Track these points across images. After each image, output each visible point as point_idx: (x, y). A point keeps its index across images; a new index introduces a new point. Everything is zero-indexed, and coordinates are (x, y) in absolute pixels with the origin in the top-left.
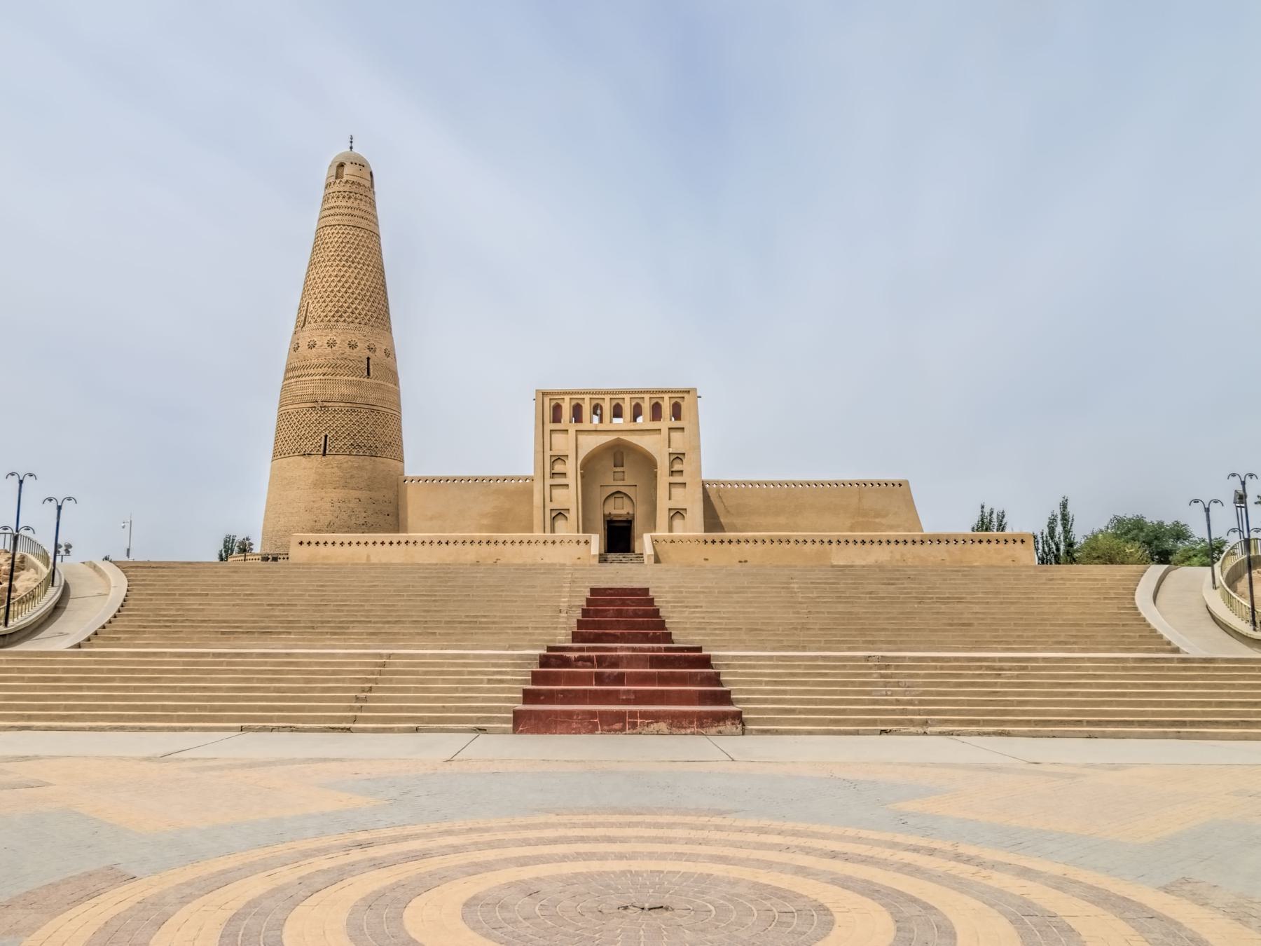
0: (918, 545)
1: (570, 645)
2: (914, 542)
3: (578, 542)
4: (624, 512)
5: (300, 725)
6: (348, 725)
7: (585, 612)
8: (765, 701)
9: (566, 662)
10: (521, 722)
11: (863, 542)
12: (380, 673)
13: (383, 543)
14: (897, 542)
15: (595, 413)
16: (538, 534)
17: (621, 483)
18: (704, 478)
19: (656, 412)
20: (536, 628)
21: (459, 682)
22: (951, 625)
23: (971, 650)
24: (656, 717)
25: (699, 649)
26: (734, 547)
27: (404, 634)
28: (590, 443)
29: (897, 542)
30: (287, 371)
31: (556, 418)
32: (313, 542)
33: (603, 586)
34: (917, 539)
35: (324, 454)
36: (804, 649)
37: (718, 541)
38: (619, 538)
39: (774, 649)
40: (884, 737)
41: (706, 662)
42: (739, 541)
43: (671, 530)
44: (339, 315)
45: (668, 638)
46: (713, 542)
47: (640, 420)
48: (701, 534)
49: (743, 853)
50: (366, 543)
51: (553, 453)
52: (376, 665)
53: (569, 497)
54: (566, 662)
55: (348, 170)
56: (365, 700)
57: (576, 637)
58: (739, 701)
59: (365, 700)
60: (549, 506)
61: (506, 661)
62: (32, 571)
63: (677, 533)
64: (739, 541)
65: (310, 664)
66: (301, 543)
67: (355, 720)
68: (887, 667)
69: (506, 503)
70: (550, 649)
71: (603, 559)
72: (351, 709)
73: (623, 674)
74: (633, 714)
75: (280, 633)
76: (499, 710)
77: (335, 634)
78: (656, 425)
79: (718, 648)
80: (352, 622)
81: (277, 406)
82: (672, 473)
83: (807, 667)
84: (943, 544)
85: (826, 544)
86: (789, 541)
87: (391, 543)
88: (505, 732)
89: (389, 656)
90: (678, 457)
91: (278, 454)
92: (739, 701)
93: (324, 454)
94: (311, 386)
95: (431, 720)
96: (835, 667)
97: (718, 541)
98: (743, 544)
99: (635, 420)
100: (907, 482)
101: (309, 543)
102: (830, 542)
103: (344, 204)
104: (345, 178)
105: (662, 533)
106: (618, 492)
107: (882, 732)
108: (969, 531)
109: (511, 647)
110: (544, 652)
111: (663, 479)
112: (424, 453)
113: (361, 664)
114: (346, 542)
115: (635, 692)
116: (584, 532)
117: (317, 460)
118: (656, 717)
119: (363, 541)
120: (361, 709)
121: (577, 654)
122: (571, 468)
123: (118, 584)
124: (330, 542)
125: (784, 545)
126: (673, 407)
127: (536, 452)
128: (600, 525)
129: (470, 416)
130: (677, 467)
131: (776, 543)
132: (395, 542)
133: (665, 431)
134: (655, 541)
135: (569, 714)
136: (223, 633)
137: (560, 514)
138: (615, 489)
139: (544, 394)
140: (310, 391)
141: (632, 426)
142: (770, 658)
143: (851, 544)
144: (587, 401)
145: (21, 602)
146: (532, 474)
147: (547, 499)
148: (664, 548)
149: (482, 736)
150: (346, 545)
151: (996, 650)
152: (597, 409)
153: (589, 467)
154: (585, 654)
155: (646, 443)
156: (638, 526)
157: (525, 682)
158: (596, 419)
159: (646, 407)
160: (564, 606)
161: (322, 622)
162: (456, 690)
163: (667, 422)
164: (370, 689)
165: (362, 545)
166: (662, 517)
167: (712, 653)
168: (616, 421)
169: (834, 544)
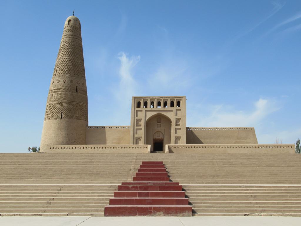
0: (257, 148)
1: (133, 182)
3: (136, 148)
5: (23, 213)
6: (41, 213)
7: (139, 170)
8: (201, 203)
9: (128, 188)
10: (109, 212)
15: (152, 105)
17: (159, 128)
18: (187, 127)
20: (121, 176)
21: (87, 196)
22: (270, 174)
23: (277, 183)
24: (159, 209)
25: (178, 183)
26: (196, 149)
27: (73, 178)
28: (149, 115)
29: (250, 147)
30: (50, 91)
31: (139, 105)
33: (147, 161)
34: (257, 146)
36: (217, 183)
37: (193, 147)
38: (158, 147)
39: (206, 183)
40: (246, 217)
41: (180, 188)
42: (197, 147)
46: (200, 147)
47: (166, 107)
48: (186, 144)
50: (72, 148)
51: (137, 118)
52: (57, 190)
53: (142, 133)
54: (128, 188)
56: (50, 203)
57: (135, 179)
59: (50, 203)
60: (136, 136)
61: (106, 188)
65: (32, 190)
66: (51, 148)
67: (45, 211)
68: (247, 190)
70: (123, 183)
71: (151, 152)
72: (44, 207)
73: (148, 193)
74: (150, 208)
75: (28, 178)
77: (48, 178)
78: (172, 108)
79: (183, 183)
80: (55, 174)
83: (218, 190)
84: (265, 148)
88: (101, 215)
89: (63, 187)
95: (74, 211)
96: (229, 190)
98: (199, 148)
100: (253, 128)
102: (228, 147)
106: (159, 131)
107: (245, 215)
109: (111, 183)
110: (121, 185)
111: (173, 126)
113: (52, 190)
114: (66, 148)
115: (153, 200)
118: (159, 209)
119: (71, 147)
120: (48, 207)
122: (143, 123)
124: (93, 148)
125: (212, 148)
126: (176, 103)
128: (152, 142)
131: (209, 148)
133: (175, 111)
134: (169, 148)
141: (164, 109)
142: (205, 186)
143: (235, 148)
148: (173, 149)
149: (93, 217)
150: (66, 149)
151: (286, 183)
152: (152, 103)
153: (149, 123)
154: (136, 185)
157: (116, 190)
158: (152, 106)
159: (169, 103)
160: (132, 168)
161: (44, 174)
162: (85, 199)
164: (53, 199)
165: (71, 149)
167: (183, 185)
168: (158, 107)
169: (229, 148)
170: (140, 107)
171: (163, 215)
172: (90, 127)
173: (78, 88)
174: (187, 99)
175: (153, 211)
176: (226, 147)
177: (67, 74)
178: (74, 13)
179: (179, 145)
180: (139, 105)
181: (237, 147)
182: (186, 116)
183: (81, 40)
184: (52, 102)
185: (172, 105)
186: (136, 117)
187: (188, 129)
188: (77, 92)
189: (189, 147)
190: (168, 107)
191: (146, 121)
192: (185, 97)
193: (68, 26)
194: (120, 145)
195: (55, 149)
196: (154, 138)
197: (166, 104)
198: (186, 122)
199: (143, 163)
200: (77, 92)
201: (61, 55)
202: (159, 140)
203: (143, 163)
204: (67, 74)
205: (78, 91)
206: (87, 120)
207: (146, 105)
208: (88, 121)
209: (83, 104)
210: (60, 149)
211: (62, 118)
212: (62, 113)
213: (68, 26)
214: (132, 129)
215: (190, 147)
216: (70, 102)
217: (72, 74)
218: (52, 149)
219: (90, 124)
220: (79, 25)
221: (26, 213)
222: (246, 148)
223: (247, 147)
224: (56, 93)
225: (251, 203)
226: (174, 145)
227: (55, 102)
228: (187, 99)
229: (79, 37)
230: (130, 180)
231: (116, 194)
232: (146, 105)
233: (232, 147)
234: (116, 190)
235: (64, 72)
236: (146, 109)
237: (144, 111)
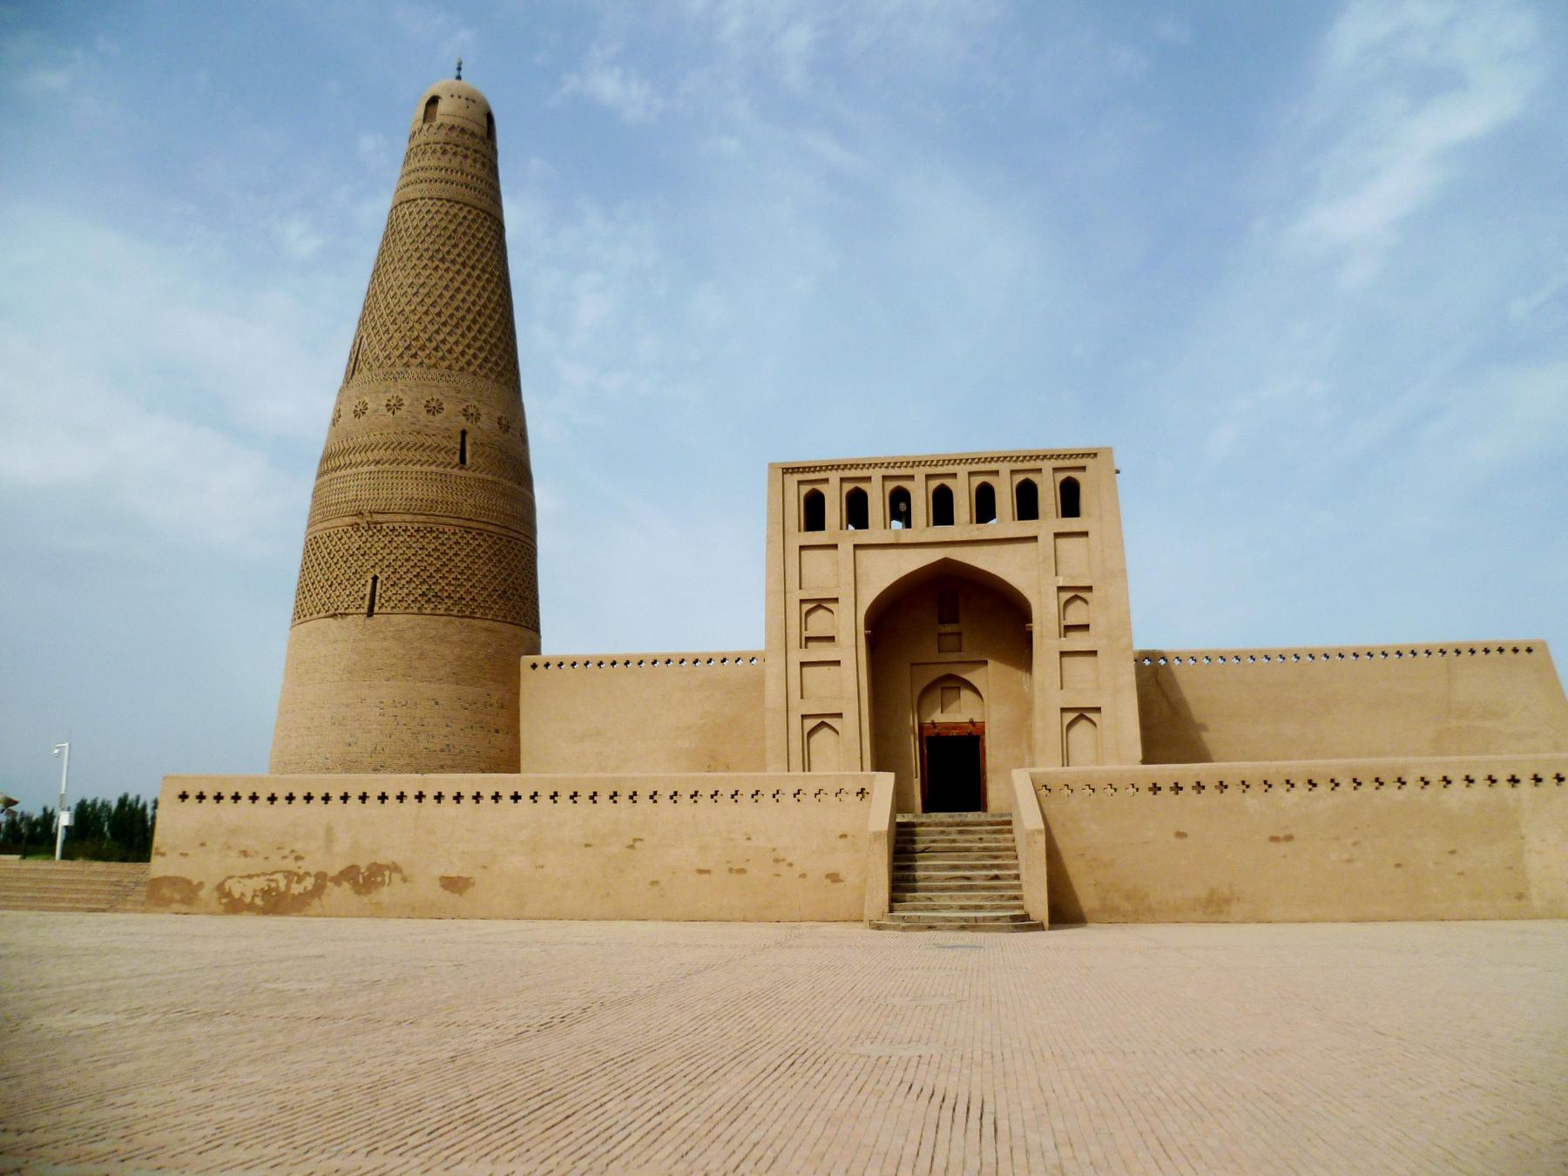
4: (962, 718)
16: (774, 774)
17: (954, 657)
19: (1027, 504)
26: (1253, 801)
28: (886, 570)
35: (370, 613)
37: (1165, 785)
43: (1066, 760)
44: (410, 352)
46: (1199, 787)
60: (799, 708)
63: (1083, 765)
66: (184, 797)
81: (305, 524)
86: (1401, 782)
87: (516, 797)
90: (1076, 593)
91: (300, 615)
93: (370, 613)
94: (357, 485)
97: (1165, 785)
98: (1280, 790)
100: (1109, 450)
105: (1050, 767)
112: (577, 607)
117: (355, 624)
122: (847, 628)
124: (373, 795)
126: (1057, 492)
127: (769, 593)
130: (1076, 615)
131: (1368, 787)
132: (506, 794)
133: (1046, 538)
134: (1043, 789)
137: (822, 722)
139: (787, 470)
140: (351, 495)
150: (281, 801)
152: (899, 505)
156: (994, 755)
163: (1050, 518)
166: (1047, 725)
170: (822, 528)
177: (407, 365)
179: (1105, 767)
180: (814, 514)
182: (1124, 572)
184: (325, 524)
187: (1147, 662)
188: (463, 460)
189: (1155, 788)
190: (1005, 522)
192: (1109, 450)
193: (426, 127)
194: (725, 781)
195: (209, 801)
197: (985, 506)
198: (1128, 612)
200: (463, 460)
202: (954, 733)
204: (407, 365)
205: (468, 462)
207: (857, 511)
208: (537, 630)
211: (376, 609)
212: (375, 579)
213: (426, 127)
214: (774, 669)
215: (1188, 786)
216: (421, 518)
217: (435, 366)
218: (192, 799)
221: (1323, 761)
224: (349, 471)
226: (1061, 769)
227: (338, 522)
232: (857, 511)
235: (406, 359)
236: (863, 536)
237: (846, 548)
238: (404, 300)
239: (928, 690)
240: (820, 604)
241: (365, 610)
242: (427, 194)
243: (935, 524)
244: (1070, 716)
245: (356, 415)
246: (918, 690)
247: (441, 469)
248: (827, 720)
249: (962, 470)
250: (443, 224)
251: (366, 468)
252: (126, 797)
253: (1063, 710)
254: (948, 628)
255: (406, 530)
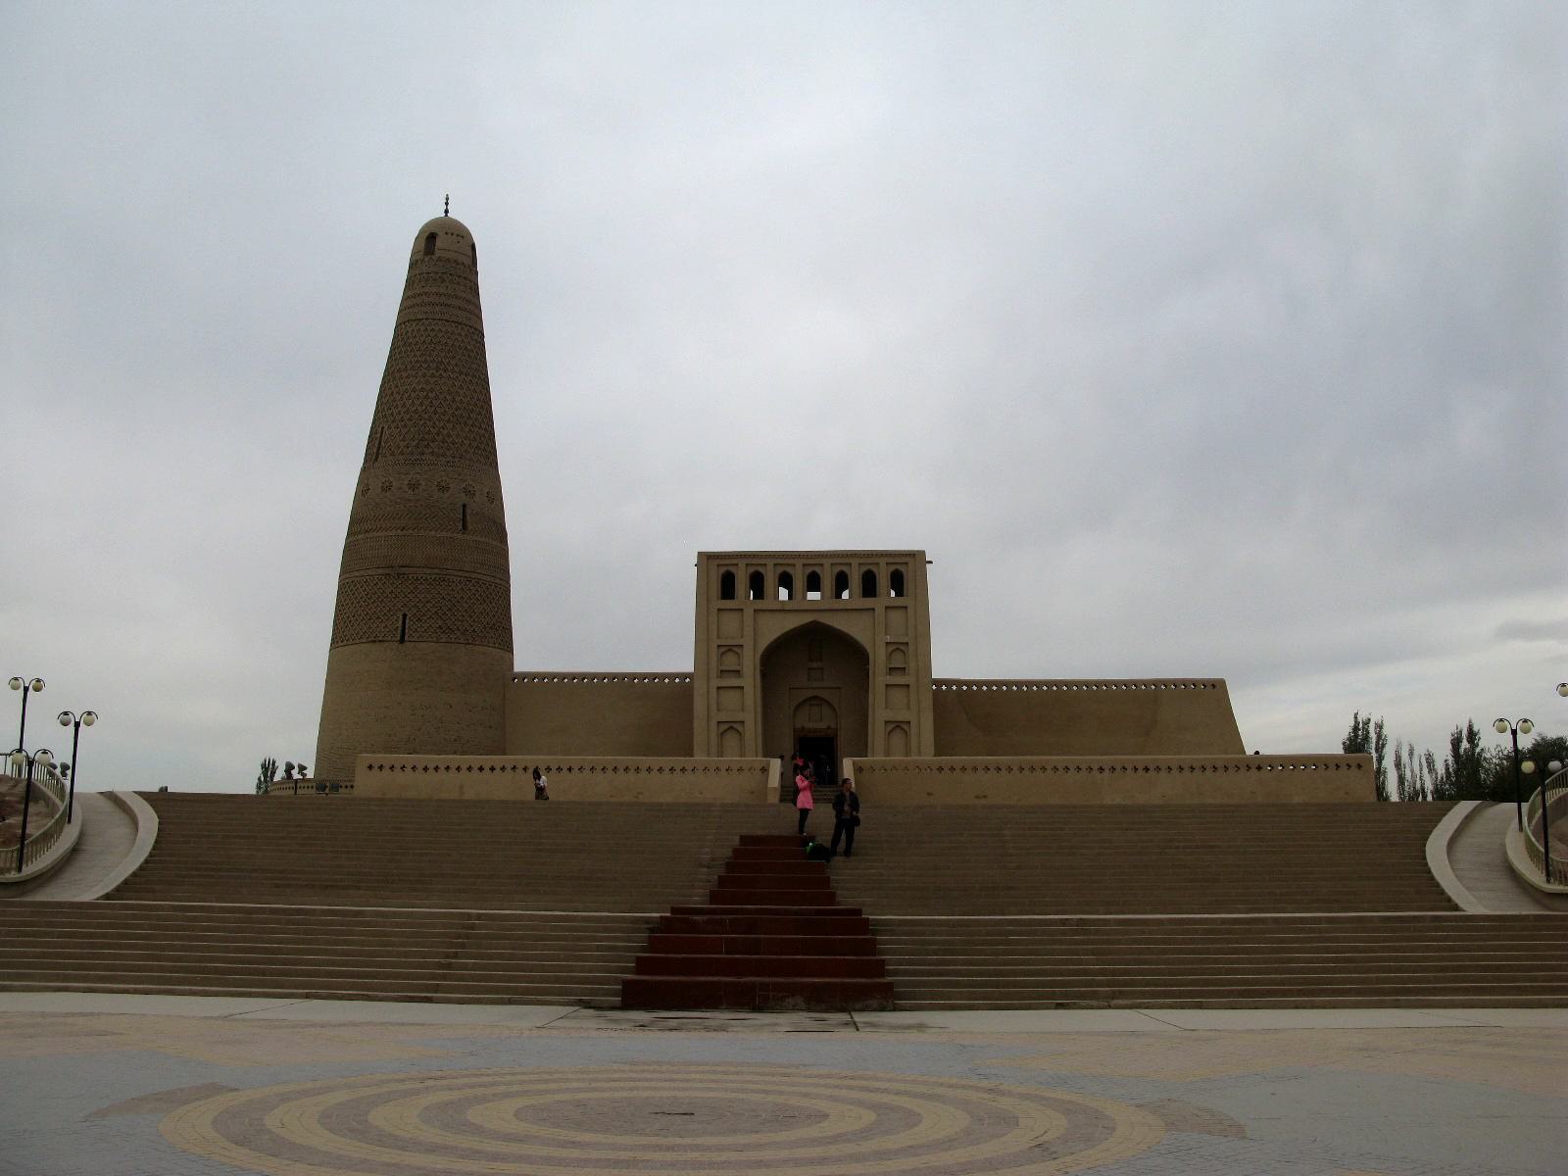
2: (1181, 769)
4: (823, 725)
7: (730, 866)
11: (1147, 769)
12: (467, 937)
13: (481, 769)
14: (1147, 769)
25: (859, 912)
32: (431, 766)
35: (402, 640)
38: (815, 755)
41: (864, 926)
45: (831, 898)
47: (845, 595)
49: (724, 1156)
50: (458, 769)
51: (889, 639)
55: (439, 243)
56: (449, 966)
57: (714, 897)
58: (896, 973)
62: (42, 802)
64: (975, 769)
69: (649, 710)
70: (674, 911)
76: (606, 981)
78: (869, 602)
82: (723, 673)
85: (1096, 773)
92: (896, 973)
93: (402, 640)
99: (839, 596)
100: (1222, 683)
101: (381, 768)
103: (434, 290)
104: (438, 254)
106: (815, 697)
108: (1340, 751)
111: (879, 678)
112: (545, 638)
116: (765, 756)
120: (444, 977)
121: (706, 917)
122: (750, 663)
123: (149, 822)
126: (894, 577)
128: (788, 745)
129: (598, 584)
135: (1544, 981)
136: (277, 886)
138: (809, 693)
141: (835, 604)
144: (770, 567)
145: (35, 842)
146: (691, 669)
147: (714, 707)
150: (431, 771)
153: (777, 659)
155: (855, 628)
156: (842, 742)
157: (623, 970)
159: (855, 580)
167: (871, 917)
171: (803, 1006)
172: (524, 676)
173: (468, 511)
174: (930, 562)
175: (771, 994)
176: (1095, 767)
178: (447, 204)
180: (728, 587)
181: (1140, 767)
183: (476, 311)
185: (869, 587)
186: (718, 637)
188: (464, 527)
191: (758, 656)
196: (798, 726)
199: (744, 839)
200: (464, 527)
201: (397, 375)
203: (744, 839)
205: (470, 527)
206: (506, 644)
207: (757, 583)
209: (488, 578)
210: (408, 770)
211: (406, 638)
212: (405, 616)
219: (528, 657)
220: (471, 254)
222: (1175, 772)
223: (1192, 768)
224: (380, 534)
225: (1086, 973)
228: (930, 562)
229: (469, 301)
230: (697, 899)
231: (653, 945)
233: (1118, 768)
234: (623, 970)
236: (760, 604)
238: (417, 402)
239: (797, 708)
240: (730, 649)
241: (399, 638)
242: (406, 320)
243: (864, 596)
244: (890, 727)
245: (384, 490)
246: (792, 709)
247: (385, 533)
248: (735, 726)
249: (742, 563)
250: (422, 339)
251: (394, 533)
252: (166, 788)
253: (886, 722)
254: (815, 665)
255: (426, 580)
